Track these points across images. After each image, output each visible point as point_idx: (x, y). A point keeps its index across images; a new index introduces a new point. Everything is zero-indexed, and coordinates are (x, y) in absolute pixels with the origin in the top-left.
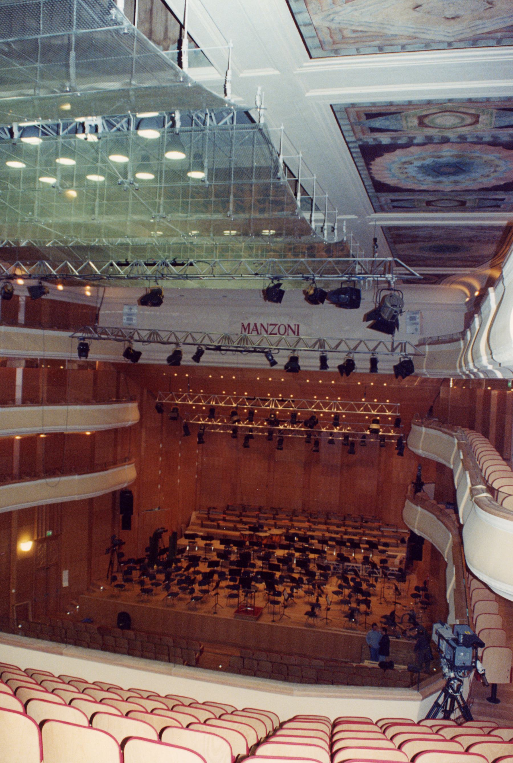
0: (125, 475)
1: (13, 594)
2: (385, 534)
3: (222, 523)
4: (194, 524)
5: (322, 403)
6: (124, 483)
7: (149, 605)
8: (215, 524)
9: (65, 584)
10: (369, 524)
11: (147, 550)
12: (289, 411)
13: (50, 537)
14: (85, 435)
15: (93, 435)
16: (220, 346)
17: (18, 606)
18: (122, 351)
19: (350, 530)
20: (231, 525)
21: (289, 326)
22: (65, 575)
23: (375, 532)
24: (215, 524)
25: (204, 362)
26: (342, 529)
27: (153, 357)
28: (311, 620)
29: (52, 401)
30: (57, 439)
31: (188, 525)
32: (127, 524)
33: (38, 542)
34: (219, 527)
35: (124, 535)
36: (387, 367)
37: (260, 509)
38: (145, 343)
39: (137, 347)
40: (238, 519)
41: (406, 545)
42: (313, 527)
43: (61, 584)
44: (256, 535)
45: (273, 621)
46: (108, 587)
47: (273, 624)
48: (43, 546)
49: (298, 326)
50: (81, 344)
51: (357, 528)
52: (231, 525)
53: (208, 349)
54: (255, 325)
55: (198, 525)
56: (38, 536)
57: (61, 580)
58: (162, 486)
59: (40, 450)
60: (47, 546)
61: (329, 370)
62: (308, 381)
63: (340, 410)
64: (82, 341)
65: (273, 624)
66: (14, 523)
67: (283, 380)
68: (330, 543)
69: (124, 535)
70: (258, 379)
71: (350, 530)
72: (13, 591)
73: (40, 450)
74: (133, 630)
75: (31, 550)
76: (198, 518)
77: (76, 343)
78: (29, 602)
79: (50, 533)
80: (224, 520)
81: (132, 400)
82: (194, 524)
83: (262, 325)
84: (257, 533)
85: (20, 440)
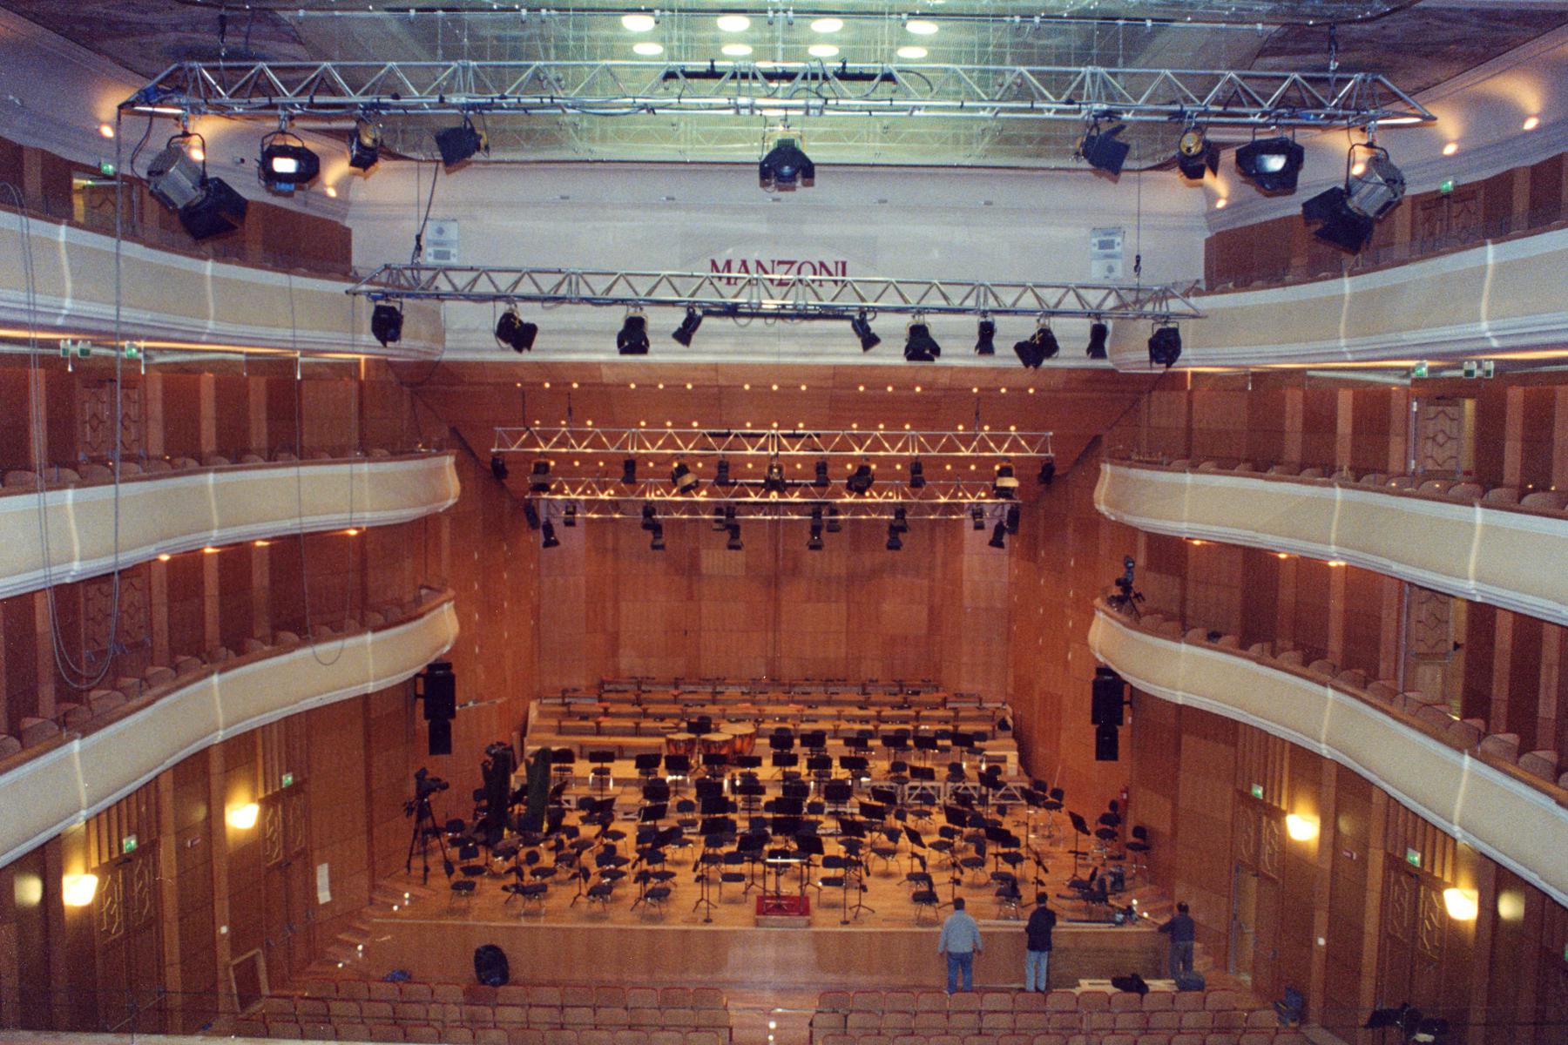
0: (441, 628)
1: (223, 936)
2: (962, 714)
3: (606, 723)
4: (537, 729)
5: (605, 447)
6: (443, 645)
7: (541, 923)
8: (591, 724)
9: (324, 896)
10: (923, 697)
11: (478, 795)
12: (852, 459)
13: (290, 788)
14: (347, 536)
15: (363, 536)
16: (736, 306)
17: (238, 965)
18: (493, 324)
19: (887, 712)
20: (629, 723)
21: (822, 265)
22: (323, 874)
23: (940, 713)
24: (591, 724)
25: (542, 351)
26: (872, 712)
27: (474, 344)
28: (928, 911)
29: (273, 456)
30: (293, 551)
31: (523, 734)
32: (440, 741)
33: (267, 803)
34: (599, 731)
35: (438, 766)
36: (960, 351)
37: (676, 683)
38: (547, 305)
39: (527, 314)
40: (638, 709)
41: (1010, 733)
42: (808, 712)
43: (316, 898)
44: (704, 741)
45: (845, 923)
46: (419, 892)
47: (845, 929)
48: (275, 812)
49: (844, 264)
50: (379, 309)
51: (901, 708)
52: (629, 723)
53: (708, 313)
54: (744, 263)
55: (549, 729)
56: (266, 790)
57: (315, 888)
58: (481, 647)
59: (260, 577)
60: (284, 810)
61: (938, 361)
62: (861, 388)
63: (991, 450)
64: (382, 303)
65: (845, 929)
66: (216, 765)
67: (804, 388)
68: (940, 742)
69: (438, 766)
70: (804, 388)
71: (887, 712)
72: (224, 930)
73: (260, 577)
74: (516, 983)
75: (253, 830)
76: (542, 715)
77: (366, 310)
78: (258, 950)
79: (288, 779)
80: (606, 713)
81: (441, 449)
82: (537, 729)
83: (759, 263)
84: (704, 736)
85: (168, 562)
